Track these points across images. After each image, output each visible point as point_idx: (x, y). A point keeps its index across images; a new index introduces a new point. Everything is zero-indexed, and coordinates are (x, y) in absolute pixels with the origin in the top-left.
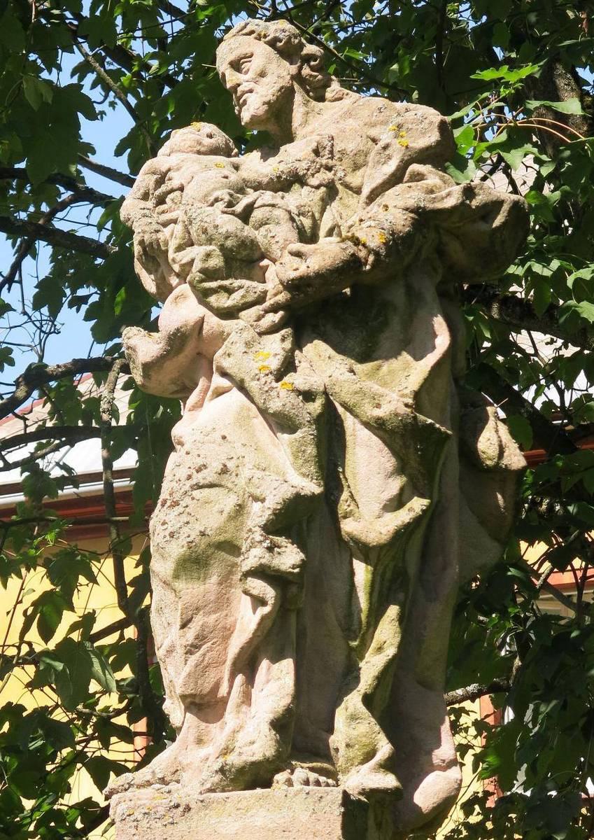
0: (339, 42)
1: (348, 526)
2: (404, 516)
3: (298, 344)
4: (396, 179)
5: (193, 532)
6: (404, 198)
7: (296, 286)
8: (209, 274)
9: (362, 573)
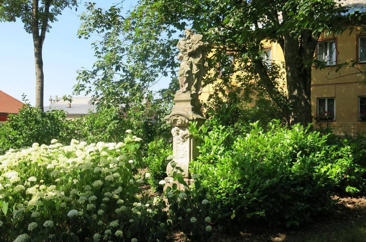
0: (256, 57)
1: (193, 72)
2: (197, 71)
3: (189, 57)
4: (198, 43)
5: (180, 73)
6: (198, 44)
7: (189, 53)
8: (182, 52)
9: (194, 76)
